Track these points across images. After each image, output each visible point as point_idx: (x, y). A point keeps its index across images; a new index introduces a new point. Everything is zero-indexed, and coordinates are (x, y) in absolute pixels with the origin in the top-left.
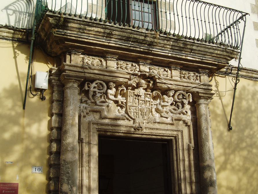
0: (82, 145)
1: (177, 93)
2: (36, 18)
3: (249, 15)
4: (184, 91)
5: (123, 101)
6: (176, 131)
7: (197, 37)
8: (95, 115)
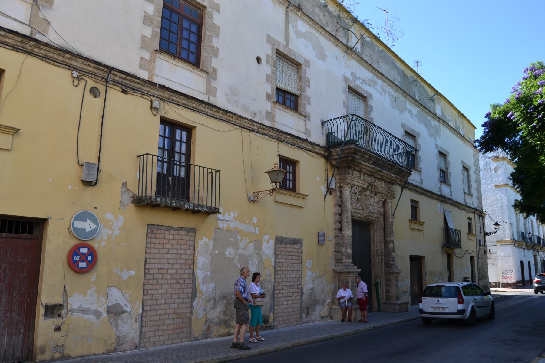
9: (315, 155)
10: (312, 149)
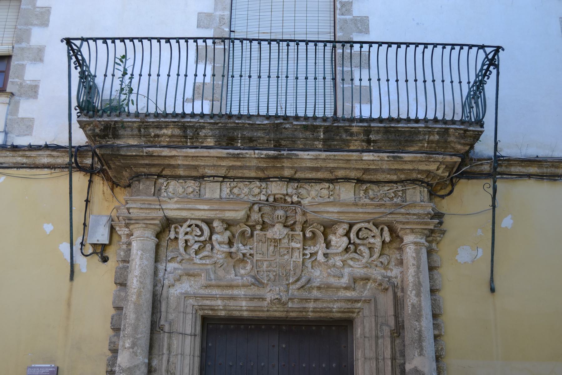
0: (195, 331)
1: (355, 228)
3: (503, 50)
5: (245, 251)
6: (284, 311)
7: (431, 116)
8: (193, 282)
9: (46, 171)
10: (24, 160)
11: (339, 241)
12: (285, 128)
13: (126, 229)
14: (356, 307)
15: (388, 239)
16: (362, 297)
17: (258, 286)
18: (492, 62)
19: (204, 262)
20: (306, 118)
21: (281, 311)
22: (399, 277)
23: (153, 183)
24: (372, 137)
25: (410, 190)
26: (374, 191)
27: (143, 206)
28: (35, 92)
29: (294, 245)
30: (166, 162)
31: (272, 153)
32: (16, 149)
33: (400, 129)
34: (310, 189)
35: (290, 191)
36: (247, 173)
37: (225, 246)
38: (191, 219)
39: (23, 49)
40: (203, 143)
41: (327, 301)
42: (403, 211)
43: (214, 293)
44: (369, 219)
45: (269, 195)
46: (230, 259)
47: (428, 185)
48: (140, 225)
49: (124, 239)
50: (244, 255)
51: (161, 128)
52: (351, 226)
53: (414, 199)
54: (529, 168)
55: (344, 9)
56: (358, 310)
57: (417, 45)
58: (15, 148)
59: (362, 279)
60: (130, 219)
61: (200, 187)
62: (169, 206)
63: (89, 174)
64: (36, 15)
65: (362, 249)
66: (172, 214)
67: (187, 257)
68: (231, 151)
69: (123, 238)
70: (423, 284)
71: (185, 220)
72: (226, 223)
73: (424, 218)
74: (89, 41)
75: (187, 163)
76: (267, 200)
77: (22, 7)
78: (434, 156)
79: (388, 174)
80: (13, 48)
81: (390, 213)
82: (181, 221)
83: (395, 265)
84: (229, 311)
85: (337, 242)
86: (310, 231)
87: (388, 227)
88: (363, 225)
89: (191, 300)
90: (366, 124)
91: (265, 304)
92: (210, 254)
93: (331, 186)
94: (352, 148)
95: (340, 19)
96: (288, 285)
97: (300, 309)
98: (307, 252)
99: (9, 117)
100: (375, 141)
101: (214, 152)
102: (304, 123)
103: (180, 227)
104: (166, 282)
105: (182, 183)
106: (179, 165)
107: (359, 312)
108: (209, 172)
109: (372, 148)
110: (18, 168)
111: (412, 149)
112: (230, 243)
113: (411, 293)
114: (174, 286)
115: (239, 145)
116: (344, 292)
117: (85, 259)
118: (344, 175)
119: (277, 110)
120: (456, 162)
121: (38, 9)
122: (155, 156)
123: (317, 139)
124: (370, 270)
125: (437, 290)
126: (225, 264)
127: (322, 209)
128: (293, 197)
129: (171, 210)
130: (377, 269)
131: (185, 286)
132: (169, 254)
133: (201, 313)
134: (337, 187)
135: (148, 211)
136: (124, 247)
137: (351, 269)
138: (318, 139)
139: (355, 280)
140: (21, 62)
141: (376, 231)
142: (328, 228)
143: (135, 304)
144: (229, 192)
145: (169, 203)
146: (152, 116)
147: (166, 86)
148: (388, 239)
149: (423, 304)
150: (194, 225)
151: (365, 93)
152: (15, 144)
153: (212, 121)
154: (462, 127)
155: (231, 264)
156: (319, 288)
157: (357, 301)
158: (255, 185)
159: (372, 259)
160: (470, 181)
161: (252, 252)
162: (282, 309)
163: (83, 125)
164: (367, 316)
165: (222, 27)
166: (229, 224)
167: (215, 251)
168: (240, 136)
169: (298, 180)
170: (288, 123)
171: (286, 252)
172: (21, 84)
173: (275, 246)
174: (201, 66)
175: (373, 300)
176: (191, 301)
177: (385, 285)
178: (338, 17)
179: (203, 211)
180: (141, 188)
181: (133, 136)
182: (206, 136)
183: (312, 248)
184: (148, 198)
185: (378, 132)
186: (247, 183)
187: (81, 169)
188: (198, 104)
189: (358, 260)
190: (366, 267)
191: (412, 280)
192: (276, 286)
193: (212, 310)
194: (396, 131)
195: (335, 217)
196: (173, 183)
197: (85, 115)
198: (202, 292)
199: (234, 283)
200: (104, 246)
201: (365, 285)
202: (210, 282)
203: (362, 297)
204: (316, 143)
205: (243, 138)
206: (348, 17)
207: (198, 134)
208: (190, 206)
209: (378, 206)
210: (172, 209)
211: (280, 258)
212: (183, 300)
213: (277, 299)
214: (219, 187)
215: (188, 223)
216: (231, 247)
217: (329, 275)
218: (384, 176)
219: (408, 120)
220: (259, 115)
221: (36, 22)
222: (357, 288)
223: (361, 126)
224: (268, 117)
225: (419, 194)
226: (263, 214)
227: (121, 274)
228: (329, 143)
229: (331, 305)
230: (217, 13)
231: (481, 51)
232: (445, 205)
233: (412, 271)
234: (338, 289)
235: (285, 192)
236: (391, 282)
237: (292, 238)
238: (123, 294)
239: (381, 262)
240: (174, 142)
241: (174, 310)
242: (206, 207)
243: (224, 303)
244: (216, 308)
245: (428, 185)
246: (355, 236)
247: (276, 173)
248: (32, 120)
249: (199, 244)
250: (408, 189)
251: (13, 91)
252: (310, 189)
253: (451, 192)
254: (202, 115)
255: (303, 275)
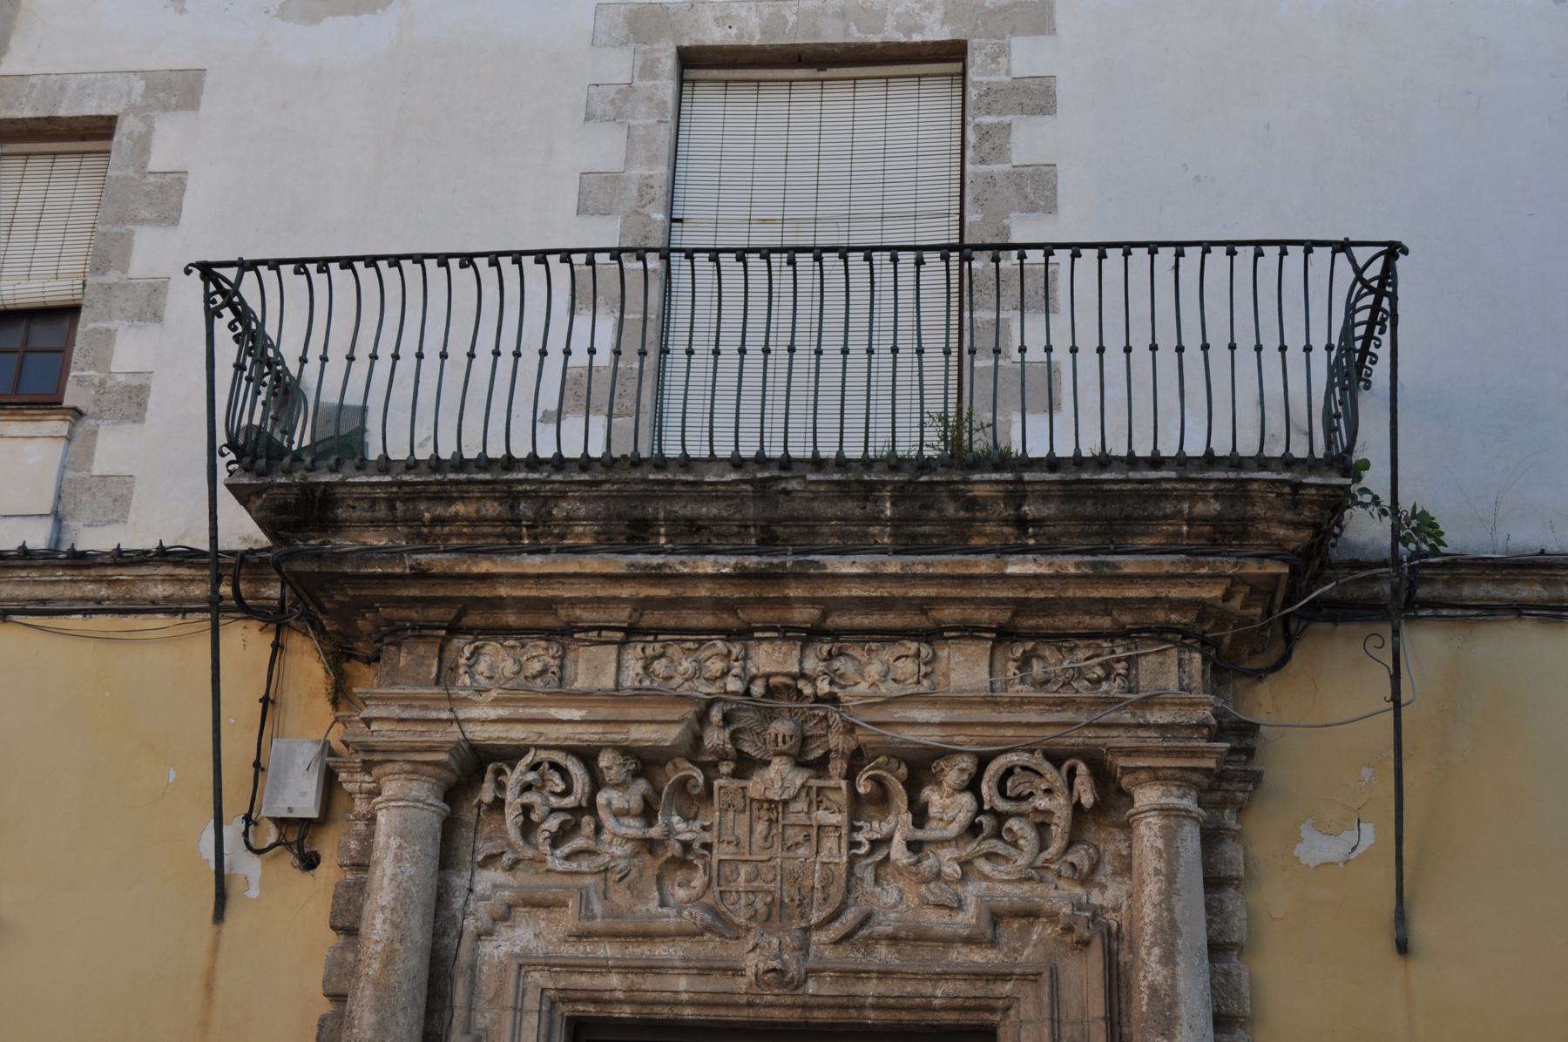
1: (995, 767)
2: (568, 623)
3: (1405, 252)
4: (1032, 751)
5: (687, 836)
6: (793, 1006)
7: (446, 453)
8: (543, 924)
9: (160, 620)
11: (949, 806)
12: (786, 492)
13: (367, 778)
14: (997, 993)
15: (1087, 799)
16: (1015, 965)
17: (722, 936)
18: (1379, 292)
19: (574, 866)
20: (841, 463)
21: (788, 1007)
22: (1124, 908)
23: (436, 650)
24: (1029, 510)
25: (1150, 658)
26: (1051, 661)
27: (405, 715)
28: (139, 404)
29: (823, 816)
30: (468, 591)
31: (751, 561)
32: (82, 562)
33: (1106, 487)
34: (864, 659)
35: (811, 664)
36: (693, 619)
37: (632, 822)
38: (538, 747)
39: (109, 288)
40: (562, 536)
41: (914, 977)
42: (1127, 717)
43: (601, 953)
44: (1031, 741)
45: (753, 678)
46: (647, 858)
47: (1205, 643)
48: (397, 767)
49: (360, 806)
50: (687, 846)
51: (451, 500)
52: (983, 761)
53: (1161, 683)
54: (1517, 586)
55: (987, 146)
56: (1007, 1002)
57: (1153, 248)
58: (80, 560)
59: (1017, 914)
60: (369, 749)
61: (562, 658)
62: (475, 713)
63: (273, 626)
64: (147, 194)
65: (1015, 828)
66: (486, 735)
67: (529, 853)
68: (641, 559)
69: (357, 802)
70: (1184, 929)
71: (522, 751)
72: (638, 758)
73: (1189, 739)
74: (260, 268)
75: (524, 593)
76: (747, 692)
77: (112, 173)
78: (1211, 559)
79: (1087, 612)
80: (84, 284)
81: (1089, 725)
82: (509, 755)
83: (1115, 873)
84: (644, 1004)
85: (944, 809)
86: (869, 778)
87: (1088, 764)
88: (1013, 758)
89: (537, 975)
90: (1008, 476)
91: (742, 984)
92: (591, 844)
93: (925, 650)
94: (976, 541)
95: (976, 174)
96: (807, 930)
97: (840, 1001)
98: (860, 837)
99: (69, 474)
100: (1038, 522)
101: (592, 564)
102: (836, 477)
103: (508, 770)
104: (470, 924)
105: (513, 647)
106: (501, 598)
107: (1008, 1008)
108: (586, 616)
109: (1031, 542)
110: (85, 612)
111: (1145, 542)
112: (648, 813)
113: (1149, 954)
114: (491, 934)
115: (663, 541)
116: (965, 950)
117: (256, 861)
118: (959, 617)
119: (762, 442)
120: (1277, 576)
121: (152, 179)
122: (433, 576)
123: (876, 519)
124: (1040, 888)
125: (1234, 945)
126: (634, 874)
127: (898, 713)
128: (818, 683)
129: (484, 722)
130: (1062, 883)
131: (522, 936)
132: (479, 844)
133: (566, 1009)
134: (943, 653)
135: (420, 728)
136: (361, 826)
137: (984, 884)
138: (879, 519)
139: (996, 917)
140: (103, 325)
141: (1054, 777)
142: (920, 768)
143: (376, 984)
144: (641, 671)
145: (474, 704)
146: (424, 467)
147: (444, 389)
148: (1087, 799)
149: (1182, 985)
150: (546, 765)
151: (1036, 379)
152: (79, 548)
153: (585, 477)
154: (1286, 476)
155: (650, 873)
156: (893, 939)
157: (1003, 977)
158: (714, 651)
159: (1046, 855)
160: (1341, 628)
161: (707, 837)
162: (789, 1000)
163: (243, 495)
164: (1031, 1022)
165: (648, 210)
166: (645, 762)
167: (606, 837)
168: (661, 515)
169: (835, 634)
170: (793, 478)
171: (800, 838)
172: (102, 383)
173: (770, 820)
174: (582, 322)
175: (1046, 974)
176: (537, 977)
177: (1082, 931)
178: (969, 167)
179: (570, 723)
180: (402, 662)
181: (375, 523)
182: (569, 518)
183: (876, 824)
184: (420, 690)
185: (1045, 498)
186: (690, 645)
187: (245, 610)
188: (573, 426)
189: (1007, 859)
190: (1030, 879)
191: (1153, 916)
192: (770, 934)
193: (595, 1001)
194: (1098, 492)
195: (932, 737)
196: (491, 647)
197: (246, 470)
198: (568, 950)
199: (656, 925)
200: (306, 826)
201: (1023, 937)
202: (587, 924)
203: (1015, 965)
204: (874, 530)
205: (672, 521)
206: (997, 168)
207: (549, 513)
208: (533, 712)
209: (1055, 704)
210: (485, 721)
211: (786, 854)
212: (513, 974)
213: (774, 970)
214: (613, 656)
215: (528, 759)
216: (650, 824)
217: (924, 902)
218: (1074, 620)
219: (1132, 461)
220: (712, 458)
221: (145, 213)
222: (1004, 940)
223: (997, 482)
224: (737, 462)
225: (1175, 668)
226: (738, 731)
227: (348, 902)
228: (910, 529)
229: (927, 989)
230: (634, 172)
231: (1341, 257)
232: (1268, 703)
233: (1152, 890)
234: (948, 941)
235: (796, 669)
236: (1100, 923)
237: (818, 798)
238: (350, 957)
239: (1072, 864)
240: (485, 536)
241: (490, 1002)
242: (577, 714)
243: (627, 983)
244: (606, 996)
245: (1204, 643)
246: (995, 790)
247: (770, 615)
248: (127, 480)
249: (561, 817)
250: (1145, 655)
251: (80, 405)
252: (864, 659)
253: (1284, 660)
254: (559, 462)
255: (851, 901)
